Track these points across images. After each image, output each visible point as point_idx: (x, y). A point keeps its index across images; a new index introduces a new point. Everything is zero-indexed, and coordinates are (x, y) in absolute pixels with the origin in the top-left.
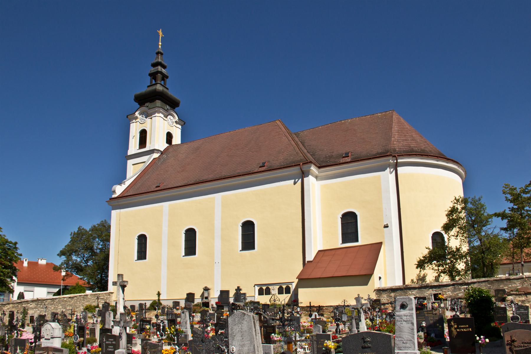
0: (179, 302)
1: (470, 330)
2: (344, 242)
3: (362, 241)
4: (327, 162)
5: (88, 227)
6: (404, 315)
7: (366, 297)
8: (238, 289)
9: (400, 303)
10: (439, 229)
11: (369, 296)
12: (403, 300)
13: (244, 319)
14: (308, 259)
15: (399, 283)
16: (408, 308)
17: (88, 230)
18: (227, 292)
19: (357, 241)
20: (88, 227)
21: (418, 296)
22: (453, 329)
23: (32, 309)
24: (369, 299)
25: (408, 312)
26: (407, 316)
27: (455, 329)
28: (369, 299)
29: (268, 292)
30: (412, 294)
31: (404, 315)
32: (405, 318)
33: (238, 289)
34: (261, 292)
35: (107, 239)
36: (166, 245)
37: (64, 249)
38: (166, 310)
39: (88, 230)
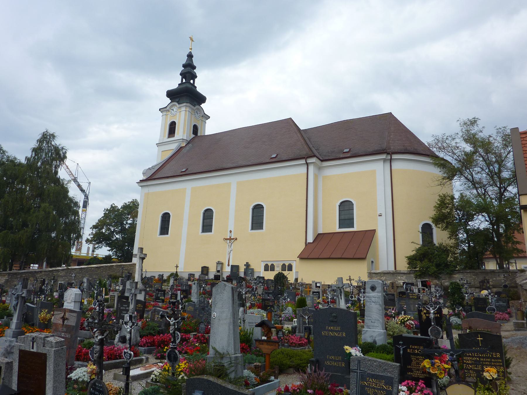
0: (194, 275)
1: (438, 315)
2: (340, 227)
3: (355, 229)
4: (329, 156)
5: (119, 205)
6: (373, 297)
7: (357, 279)
8: (247, 265)
9: (370, 285)
10: (430, 222)
11: (360, 277)
12: (373, 283)
13: (224, 289)
14: (308, 241)
15: (392, 268)
16: (376, 291)
17: (120, 207)
18: (237, 267)
19: (353, 227)
20: (119, 205)
21: (406, 281)
22: (422, 314)
23: (62, 277)
24: (360, 280)
25: (376, 294)
26: (375, 298)
27: (425, 313)
28: (360, 280)
29: (272, 268)
30: (401, 279)
31: (373, 297)
32: (373, 299)
33: (247, 265)
34: (266, 268)
35: (135, 216)
36: (186, 223)
37: (98, 223)
38: (501, 303)
39: (120, 207)
